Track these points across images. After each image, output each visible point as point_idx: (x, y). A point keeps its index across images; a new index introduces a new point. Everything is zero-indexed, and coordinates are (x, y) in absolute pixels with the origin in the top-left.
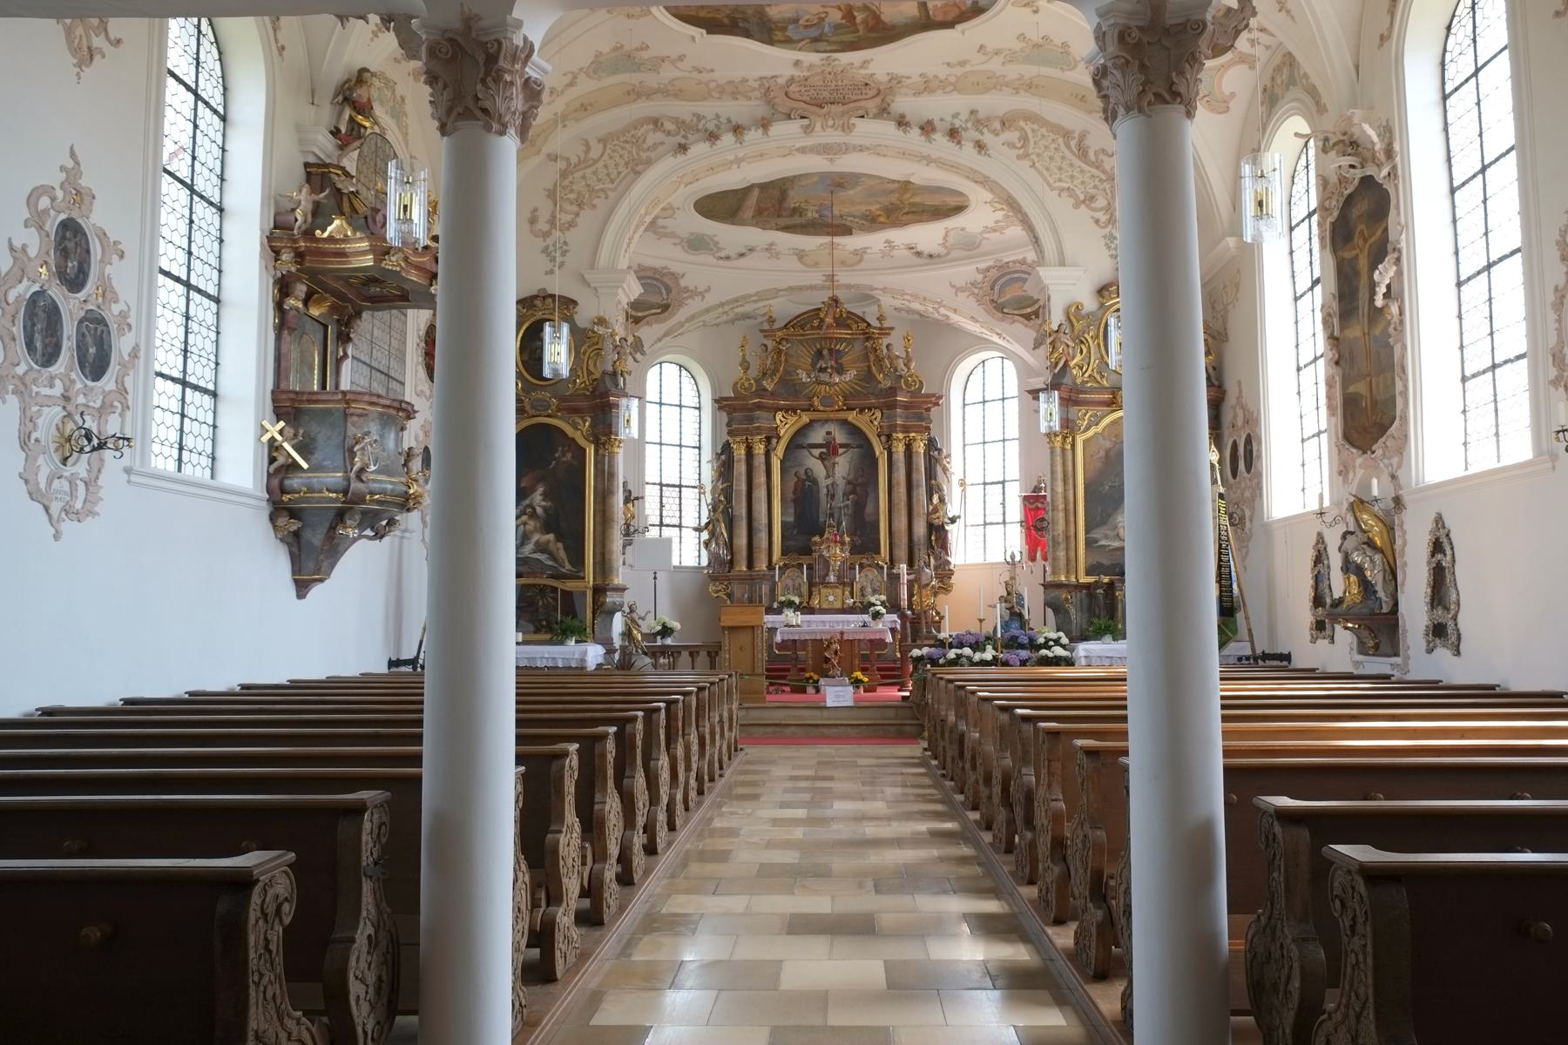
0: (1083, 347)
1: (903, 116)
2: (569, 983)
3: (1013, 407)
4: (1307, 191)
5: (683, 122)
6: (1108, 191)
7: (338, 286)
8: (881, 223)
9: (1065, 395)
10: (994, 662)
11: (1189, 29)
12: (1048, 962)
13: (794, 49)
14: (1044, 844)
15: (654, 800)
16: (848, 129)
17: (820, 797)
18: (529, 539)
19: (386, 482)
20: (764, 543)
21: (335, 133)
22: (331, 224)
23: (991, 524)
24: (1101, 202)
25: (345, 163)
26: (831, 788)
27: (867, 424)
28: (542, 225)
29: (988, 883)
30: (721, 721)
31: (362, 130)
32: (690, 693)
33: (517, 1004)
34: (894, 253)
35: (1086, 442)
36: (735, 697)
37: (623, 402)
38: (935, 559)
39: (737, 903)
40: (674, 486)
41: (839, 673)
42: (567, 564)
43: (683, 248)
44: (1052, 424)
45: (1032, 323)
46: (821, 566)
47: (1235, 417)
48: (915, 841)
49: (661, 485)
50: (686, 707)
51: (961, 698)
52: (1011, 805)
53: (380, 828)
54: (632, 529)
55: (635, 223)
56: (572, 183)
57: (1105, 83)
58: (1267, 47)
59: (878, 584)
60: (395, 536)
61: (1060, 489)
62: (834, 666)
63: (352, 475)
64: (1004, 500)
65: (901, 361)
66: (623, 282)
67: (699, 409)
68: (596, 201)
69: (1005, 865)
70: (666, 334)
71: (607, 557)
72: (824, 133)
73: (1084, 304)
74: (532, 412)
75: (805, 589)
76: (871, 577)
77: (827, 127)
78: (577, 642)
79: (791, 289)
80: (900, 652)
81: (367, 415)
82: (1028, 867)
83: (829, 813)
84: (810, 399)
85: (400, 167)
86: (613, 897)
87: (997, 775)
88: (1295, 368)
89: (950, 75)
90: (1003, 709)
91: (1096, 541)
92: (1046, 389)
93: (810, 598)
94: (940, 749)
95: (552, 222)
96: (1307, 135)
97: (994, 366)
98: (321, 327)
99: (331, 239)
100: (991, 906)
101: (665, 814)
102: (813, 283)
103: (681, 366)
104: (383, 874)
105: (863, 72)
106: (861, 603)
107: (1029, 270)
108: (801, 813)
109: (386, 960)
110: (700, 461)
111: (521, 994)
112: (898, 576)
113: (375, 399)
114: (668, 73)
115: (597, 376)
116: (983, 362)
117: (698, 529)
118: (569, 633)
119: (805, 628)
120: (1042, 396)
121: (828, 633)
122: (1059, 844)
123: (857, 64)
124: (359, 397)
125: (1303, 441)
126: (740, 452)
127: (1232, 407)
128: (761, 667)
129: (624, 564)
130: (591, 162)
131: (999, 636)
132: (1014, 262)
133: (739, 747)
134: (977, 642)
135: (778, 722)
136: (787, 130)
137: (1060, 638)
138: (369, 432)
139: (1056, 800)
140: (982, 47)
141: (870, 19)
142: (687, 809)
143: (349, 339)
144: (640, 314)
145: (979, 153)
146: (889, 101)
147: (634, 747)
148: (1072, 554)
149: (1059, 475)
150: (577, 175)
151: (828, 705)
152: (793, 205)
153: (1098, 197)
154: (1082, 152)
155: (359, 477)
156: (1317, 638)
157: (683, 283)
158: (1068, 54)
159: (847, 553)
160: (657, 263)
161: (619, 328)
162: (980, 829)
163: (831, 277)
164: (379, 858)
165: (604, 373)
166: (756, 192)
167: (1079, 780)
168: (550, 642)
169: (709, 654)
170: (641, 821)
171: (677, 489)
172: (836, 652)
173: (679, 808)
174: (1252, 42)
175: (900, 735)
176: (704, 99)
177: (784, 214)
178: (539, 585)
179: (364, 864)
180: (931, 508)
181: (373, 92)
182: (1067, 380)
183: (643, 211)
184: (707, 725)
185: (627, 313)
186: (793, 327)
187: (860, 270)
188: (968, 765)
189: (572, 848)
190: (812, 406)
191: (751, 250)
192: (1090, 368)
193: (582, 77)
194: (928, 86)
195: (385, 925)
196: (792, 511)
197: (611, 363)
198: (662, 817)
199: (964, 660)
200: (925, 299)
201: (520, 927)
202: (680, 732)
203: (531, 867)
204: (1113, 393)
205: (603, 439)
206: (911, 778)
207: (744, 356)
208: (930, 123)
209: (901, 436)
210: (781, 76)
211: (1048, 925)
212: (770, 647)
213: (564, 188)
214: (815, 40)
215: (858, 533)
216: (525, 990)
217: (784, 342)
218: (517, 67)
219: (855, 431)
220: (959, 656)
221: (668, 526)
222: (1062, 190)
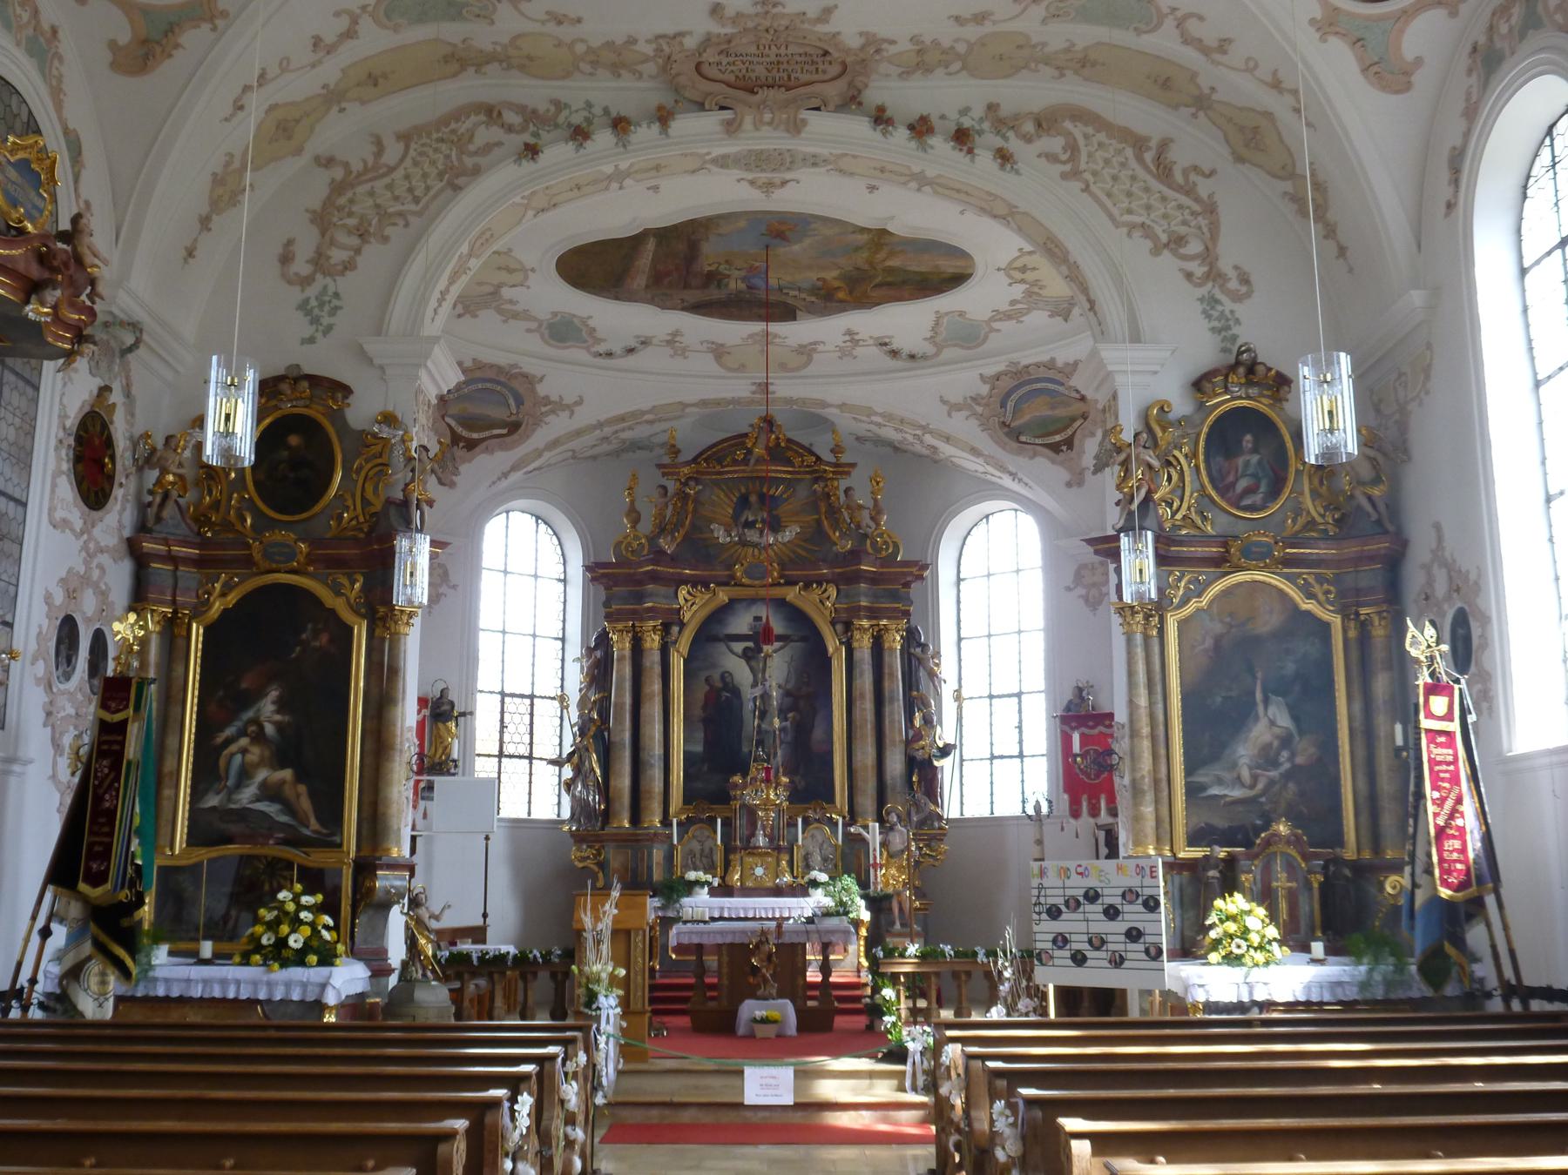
0: (1172, 471)
1: (881, 109)
5: (534, 112)
8: (841, 301)
16: (796, 127)
20: (657, 786)
23: (1002, 757)
24: (1195, 247)
27: (821, 604)
28: (301, 267)
34: (859, 351)
35: (1182, 624)
40: (522, 696)
41: (774, 992)
42: (313, 822)
43: (542, 337)
45: (1062, 456)
46: (744, 821)
47: (1430, 581)
49: (503, 694)
56: (351, 201)
61: (1143, 701)
62: (765, 980)
64: (1020, 722)
65: (866, 514)
67: (564, 581)
68: (388, 231)
73: (1172, 401)
84: (730, 567)
88: (1542, 497)
89: (957, 40)
91: (1203, 788)
103: (538, 518)
107: (1058, 377)
110: (563, 660)
117: (557, 762)
120: (1125, 541)
126: (621, 645)
127: (1424, 566)
132: (1038, 365)
135: (667, 1099)
136: (695, 127)
144: (475, 436)
145: (1002, 166)
149: (1141, 677)
150: (361, 189)
154: (1163, 170)
157: (541, 390)
161: (421, 434)
163: (765, 387)
166: (651, 245)
171: (528, 701)
176: (567, 75)
178: (266, 857)
180: (911, 733)
183: (465, 249)
186: (706, 460)
187: (801, 377)
190: (733, 577)
191: (645, 343)
192: (1185, 505)
196: (700, 735)
197: (401, 486)
204: (1225, 545)
205: (382, 610)
207: (632, 502)
208: (924, 119)
209: (865, 623)
210: (690, 33)
217: (692, 483)
219: (797, 616)
221: (511, 756)
222: (1132, 227)
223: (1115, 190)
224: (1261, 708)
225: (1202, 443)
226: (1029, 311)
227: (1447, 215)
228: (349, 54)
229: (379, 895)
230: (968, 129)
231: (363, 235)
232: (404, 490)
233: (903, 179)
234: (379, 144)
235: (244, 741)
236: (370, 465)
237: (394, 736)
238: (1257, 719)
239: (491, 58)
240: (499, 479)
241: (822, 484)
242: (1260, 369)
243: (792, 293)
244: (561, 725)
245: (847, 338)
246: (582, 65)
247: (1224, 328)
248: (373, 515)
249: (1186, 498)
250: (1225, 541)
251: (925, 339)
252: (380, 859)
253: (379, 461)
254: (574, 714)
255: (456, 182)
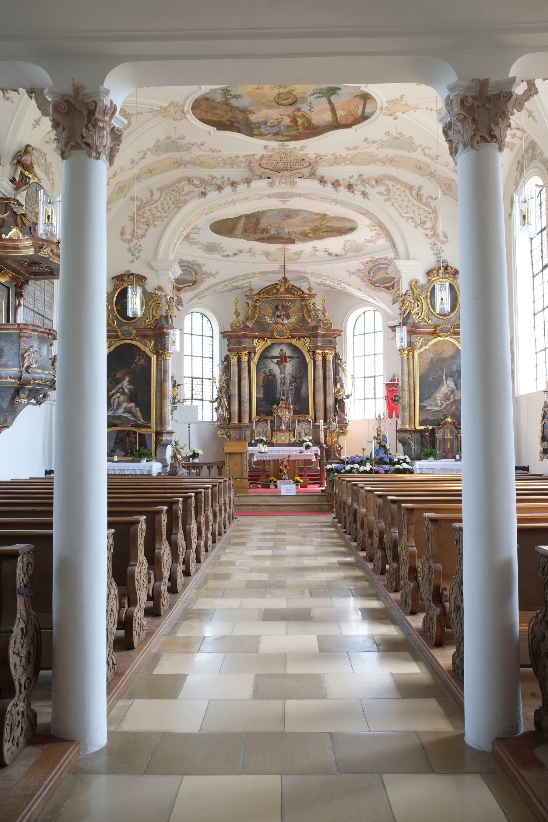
0: (419, 303)
1: (323, 177)
2: (141, 650)
3: (380, 337)
4: (541, 217)
5: (204, 180)
6: (433, 219)
7: (15, 266)
9: (410, 329)
10: (371, 471)
11: (502, 98)
12: (408, 636)
13: (264, 139)
14: (404, 570)
15: (188, 546)
16: (293, 184)
17: (278, 544)
18: (121, 406)
19: (42, 374)
20: (247, 409)
21: (13, 181)
22: (10, 231)
23: (368, 399)
24: (429, 225)
25: (18, 198)
26: (284, 539)
27: (303, 345)
28: (128, 236)
29: (372, 591)
30: (225, 503)
31: (28, 180)
32: (208, 488)
33: (111, 664)
34: (317, 253)
36: (232, 490)
37: (171, 331)
38: (338, 417)
39: (234, 603)
40: (199, 378)
41: (287, 477)
42: (141, 419)
44: (403, 344)
45: (390, 291)
46: (278, 421)
48: (329, 568)
49: (192, 378)
50: (206, 495)
51: (355, 490)
52: (384, 549)
53: (28, 566)
54: (176, 401)
55: (177, 235)
56: (143, 213)
57: (450, 133)
58: (521, 139)
59: (308, 431)
60: (48, 403)
61: (406, 379)
62: (284, 474)
63: (24, 369)
64: (375, 386)
65: (320, 312)
66: (171, 267)
68: (157, 223)
69: (381, 581)
70: (194, 297)
71: (163, 415)
72: (280, 187)
74: (122, 337)
75: (269, 433)
76: (304, 427)
77: (282, 183)
78: (147, 461)
79: (262, 273)
80: (320, 466)
81: (31, 337)
82: (394, 582)
83: (283, 552)
84: (272, 332)
85: (45, 193)
86: (166, 600)
87: (376, 532)
88: (533, 314)
90: (380, 496)
91: (425, 407)
92: (400, 325)
93: (271, 438)
94: (343, 518)
95: (133, 234)
96: (542, 186)
97: (370, 315)
98: (6, 289)
99: (11, 239)
100: (375, 604)
101: (195, 554)
102: (274, 270)
103: (203, 314)
104: (30, 592)
105: (301, 152)
106: (299, 440)
107: (389, 263)
108: (269, 553)
109: (33, 641)
110: (213, 365)
111: (113, 657)
112: (319, 427)
113: (35, 328)
114: (195, 152)
115: (158, 318)
116: (364, 312)
117: (212, 402)
118: (142, 456)
119: (269, 453)
120: (398, 329)
121: (282, 456)
122: (413, 571)
123: (298, 148)
124: (27, 327)
125: (536, 353)
126: (234, 360)
128: (246, 474)
129: (172, 419)
130: (154, 201)
131: (373, 457)
133: (235, 517)
134: (361, 461)
135: (255, 504)
136: (260, 185)
137: (406, 459)
138: (33, 346)
139: (411, 546)
140: (366, 139)
141: (305, 123)
142: (207, 551)
143: (21, 296)
144: (181, 286)
145: (364, 197)
146: (315, 169)
147: (177, 518)
148: (412, 414)
150: (147, 208)
151: (282, 495)
152: (263, 227)
153: (427, 222)
154: (419, 197)
155: (27, 371)
156: (543, 458)
157: (204, 269)
158: (412, 143)
159: (292, 414)
160: (190, 259)
161: (170, 293)
162: (366, 561)
164: (28, 583)
165: (161, 316)
166: (243, 220)
167: (427, 536)
168: (132, 461)
169: (218, 467)
170: (181, 558)
171: (201, 380)
172: (286, 467)
173: (203, 550)
174: (513, 136)
175: (320, 510)
176: (215, 167)
177: (258, 232)
178: (127, 430)
179: (18, 587)
180: (336, 390)
181: (33, 158)
182: (411, 321)
183: (182, 229)
184: (217, 505)
185: (173, 285)
186: (263, 293)
188: (359, 527)
189: (142, 574)
190: (273, 336)
192: (423, 315)
193: (149, 154)
194: (336, 161)
195: (32, 622)
196: (262, 392)
197: (165, 311)
198: (193, 555)
199: (355, 470)
200: (333, 279)
201: (112, 620)
202: (203, 509)
203: (118, 585)
204: (435, 328)
205: (161, 352)
206: (326, 533)
207: (236, 309)
208: (337, 181)
209: (320, 352)
210: (257, 154)
211: (407, 615)
212: (250, 464)
213: (139, 215)
214: (276, 134)
215: (297, 403)
216: (116, 655)
217: (258, 302)
218: (107, 119)
219: (296, 349)
220: (352, 469)
221: (196, 400)
223: (402, 205)
224: (445, 381)
225: (429, 294)
226: (378, 239)
227: (509, 218)
228: (143, 163)
229: (163, 442)
230: (352, 184)
231: (148, 225)
232: (166, 312)
233: (331, 201)
234: (152, 192)
235: (118, 394)
236: (154, 304)
237: (166, 392)
238: (443, 385)
239: (189, 163)
240: (189, 301)
241: (305, 302)
242: (449, 268)
243: (293, 235)
244: (213, 389)
245: (313, 249)
246: (220, 164)
247: (438, 254)
248: (156, 320)
249: (423, 312)
250: (435, 327)
251: (341, 249)
252: (164, 430)
253: (157, 302)
254: (218, 384)
255: (178, 205)
